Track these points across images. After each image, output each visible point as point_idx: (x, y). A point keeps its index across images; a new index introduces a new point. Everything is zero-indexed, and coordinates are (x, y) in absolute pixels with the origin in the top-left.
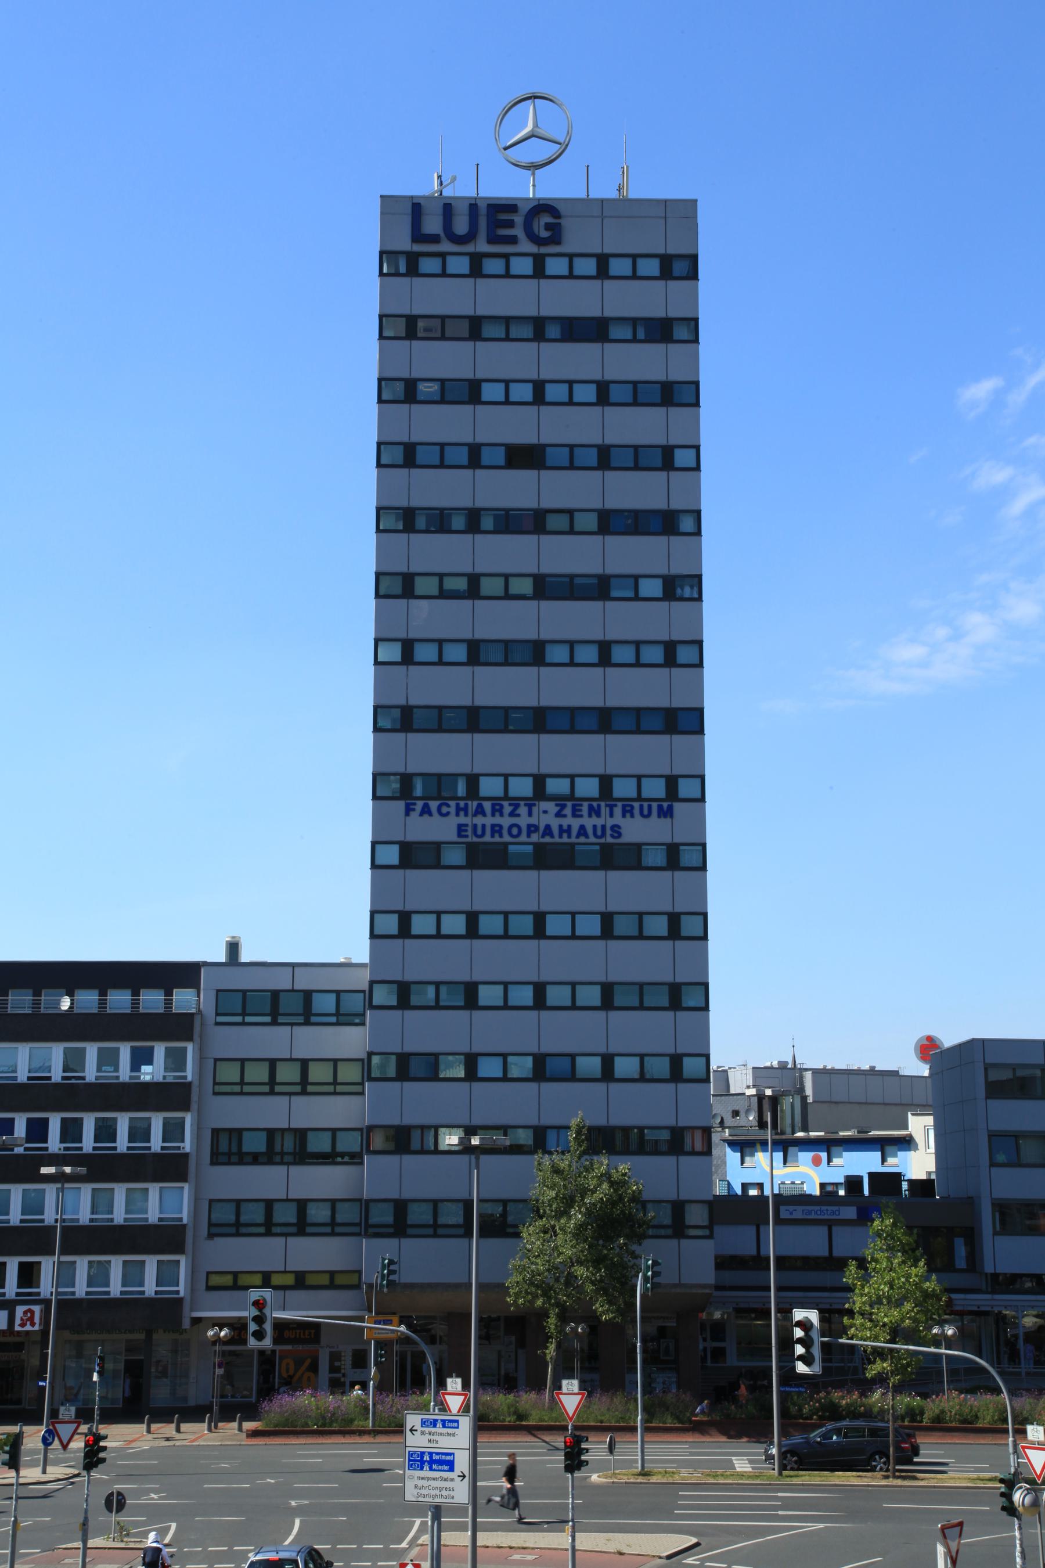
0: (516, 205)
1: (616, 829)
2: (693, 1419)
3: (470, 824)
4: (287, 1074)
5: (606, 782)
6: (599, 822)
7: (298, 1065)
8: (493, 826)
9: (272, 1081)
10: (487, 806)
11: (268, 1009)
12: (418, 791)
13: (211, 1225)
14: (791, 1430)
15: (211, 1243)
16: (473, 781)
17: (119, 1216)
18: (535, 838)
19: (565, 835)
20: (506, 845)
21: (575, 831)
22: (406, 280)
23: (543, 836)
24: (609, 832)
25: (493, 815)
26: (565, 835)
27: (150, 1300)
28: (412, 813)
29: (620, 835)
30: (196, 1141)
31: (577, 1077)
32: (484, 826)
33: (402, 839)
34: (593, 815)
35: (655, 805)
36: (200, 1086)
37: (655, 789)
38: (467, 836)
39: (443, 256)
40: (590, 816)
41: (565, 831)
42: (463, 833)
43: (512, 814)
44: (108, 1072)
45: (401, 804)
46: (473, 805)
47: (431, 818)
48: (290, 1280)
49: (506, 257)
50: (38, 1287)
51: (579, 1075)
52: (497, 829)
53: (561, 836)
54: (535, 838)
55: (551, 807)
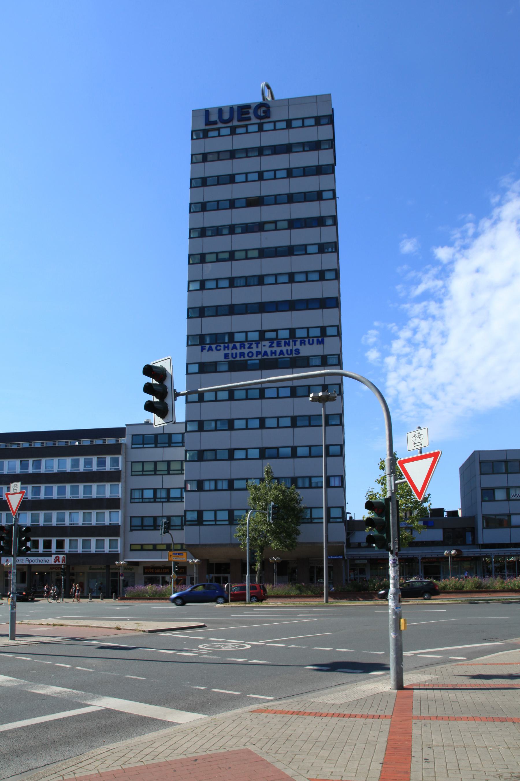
0: (250, 105)
1: (297, 350)
2: (321, 592)
3: (230, 353)
4: (162, 467)
5: (292, 331)
6: (289, 348)
7: (166, 463)
8: (240, 353)
9: (155, 470)
10: (238, 345)
11: (153, 441)
12: (208, 341)
13: (131, 526)
14: (374, 596)
15: (131, 533)
16: (231, 335)
17: (94, 522)
18: (260, 357)
19: (274, 355)
20: (247, 361)
21: (278, 353)
22: (203, 140)
23: (263, 356)
24: (294, 352)
25: (241, 349)
26: (274, 355)
27: (107, 554)
28: (204, 351)
29: (299, 353)
30: (124, 494)
31: (280, 456)
32: (236, 354)
33: (200, 361)
34: (287, 345)
35: (315, 339)
36: (126, 472)
37: (316, 332)
38: (229, 358)
39: (218, 129)
40: (285, 346)
41: (273, 353)
42: (227, 357)
43: (249, 348)
44: (88, 468)
45: (199, 347)
46: (231, 345)
47: (212, 352)
48: (165, 547)
49: (246, 126)
50: (64, 549)
51: (280, 456)
52: (242, 354)
53: (271, 355)
54: (260, 357)
55: (267, 343)
